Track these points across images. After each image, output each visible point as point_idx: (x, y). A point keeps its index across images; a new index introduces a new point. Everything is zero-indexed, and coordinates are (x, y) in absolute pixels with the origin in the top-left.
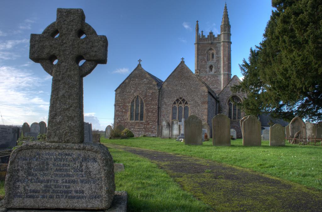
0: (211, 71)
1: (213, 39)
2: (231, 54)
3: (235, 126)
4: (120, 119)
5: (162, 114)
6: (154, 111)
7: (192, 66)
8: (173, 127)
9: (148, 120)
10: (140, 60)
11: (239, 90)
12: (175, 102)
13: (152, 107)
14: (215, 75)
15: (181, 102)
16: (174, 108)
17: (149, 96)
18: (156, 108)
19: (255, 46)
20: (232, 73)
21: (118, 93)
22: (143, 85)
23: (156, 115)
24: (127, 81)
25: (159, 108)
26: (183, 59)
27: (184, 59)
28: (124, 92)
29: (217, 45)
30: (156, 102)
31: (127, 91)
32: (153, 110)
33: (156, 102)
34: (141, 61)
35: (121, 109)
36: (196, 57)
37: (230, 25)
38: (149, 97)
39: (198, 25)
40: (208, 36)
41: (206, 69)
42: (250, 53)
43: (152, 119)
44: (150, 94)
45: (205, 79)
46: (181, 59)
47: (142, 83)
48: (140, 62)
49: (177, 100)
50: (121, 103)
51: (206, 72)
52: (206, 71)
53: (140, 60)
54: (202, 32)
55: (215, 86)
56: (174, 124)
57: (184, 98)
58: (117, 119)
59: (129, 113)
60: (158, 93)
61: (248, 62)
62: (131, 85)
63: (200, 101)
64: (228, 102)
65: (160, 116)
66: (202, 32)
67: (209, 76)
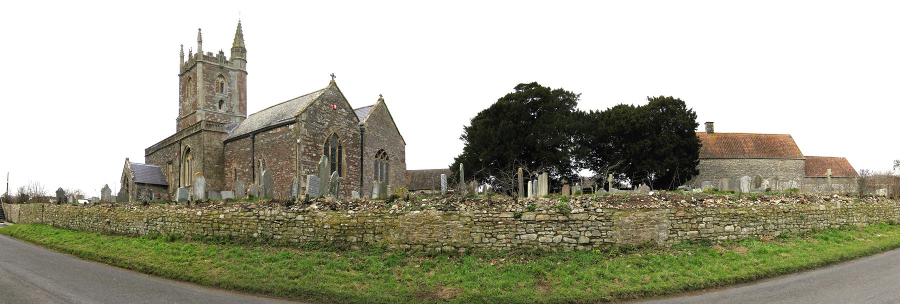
16: (376, 166)
35: (310, 151)
39: (200, 34)
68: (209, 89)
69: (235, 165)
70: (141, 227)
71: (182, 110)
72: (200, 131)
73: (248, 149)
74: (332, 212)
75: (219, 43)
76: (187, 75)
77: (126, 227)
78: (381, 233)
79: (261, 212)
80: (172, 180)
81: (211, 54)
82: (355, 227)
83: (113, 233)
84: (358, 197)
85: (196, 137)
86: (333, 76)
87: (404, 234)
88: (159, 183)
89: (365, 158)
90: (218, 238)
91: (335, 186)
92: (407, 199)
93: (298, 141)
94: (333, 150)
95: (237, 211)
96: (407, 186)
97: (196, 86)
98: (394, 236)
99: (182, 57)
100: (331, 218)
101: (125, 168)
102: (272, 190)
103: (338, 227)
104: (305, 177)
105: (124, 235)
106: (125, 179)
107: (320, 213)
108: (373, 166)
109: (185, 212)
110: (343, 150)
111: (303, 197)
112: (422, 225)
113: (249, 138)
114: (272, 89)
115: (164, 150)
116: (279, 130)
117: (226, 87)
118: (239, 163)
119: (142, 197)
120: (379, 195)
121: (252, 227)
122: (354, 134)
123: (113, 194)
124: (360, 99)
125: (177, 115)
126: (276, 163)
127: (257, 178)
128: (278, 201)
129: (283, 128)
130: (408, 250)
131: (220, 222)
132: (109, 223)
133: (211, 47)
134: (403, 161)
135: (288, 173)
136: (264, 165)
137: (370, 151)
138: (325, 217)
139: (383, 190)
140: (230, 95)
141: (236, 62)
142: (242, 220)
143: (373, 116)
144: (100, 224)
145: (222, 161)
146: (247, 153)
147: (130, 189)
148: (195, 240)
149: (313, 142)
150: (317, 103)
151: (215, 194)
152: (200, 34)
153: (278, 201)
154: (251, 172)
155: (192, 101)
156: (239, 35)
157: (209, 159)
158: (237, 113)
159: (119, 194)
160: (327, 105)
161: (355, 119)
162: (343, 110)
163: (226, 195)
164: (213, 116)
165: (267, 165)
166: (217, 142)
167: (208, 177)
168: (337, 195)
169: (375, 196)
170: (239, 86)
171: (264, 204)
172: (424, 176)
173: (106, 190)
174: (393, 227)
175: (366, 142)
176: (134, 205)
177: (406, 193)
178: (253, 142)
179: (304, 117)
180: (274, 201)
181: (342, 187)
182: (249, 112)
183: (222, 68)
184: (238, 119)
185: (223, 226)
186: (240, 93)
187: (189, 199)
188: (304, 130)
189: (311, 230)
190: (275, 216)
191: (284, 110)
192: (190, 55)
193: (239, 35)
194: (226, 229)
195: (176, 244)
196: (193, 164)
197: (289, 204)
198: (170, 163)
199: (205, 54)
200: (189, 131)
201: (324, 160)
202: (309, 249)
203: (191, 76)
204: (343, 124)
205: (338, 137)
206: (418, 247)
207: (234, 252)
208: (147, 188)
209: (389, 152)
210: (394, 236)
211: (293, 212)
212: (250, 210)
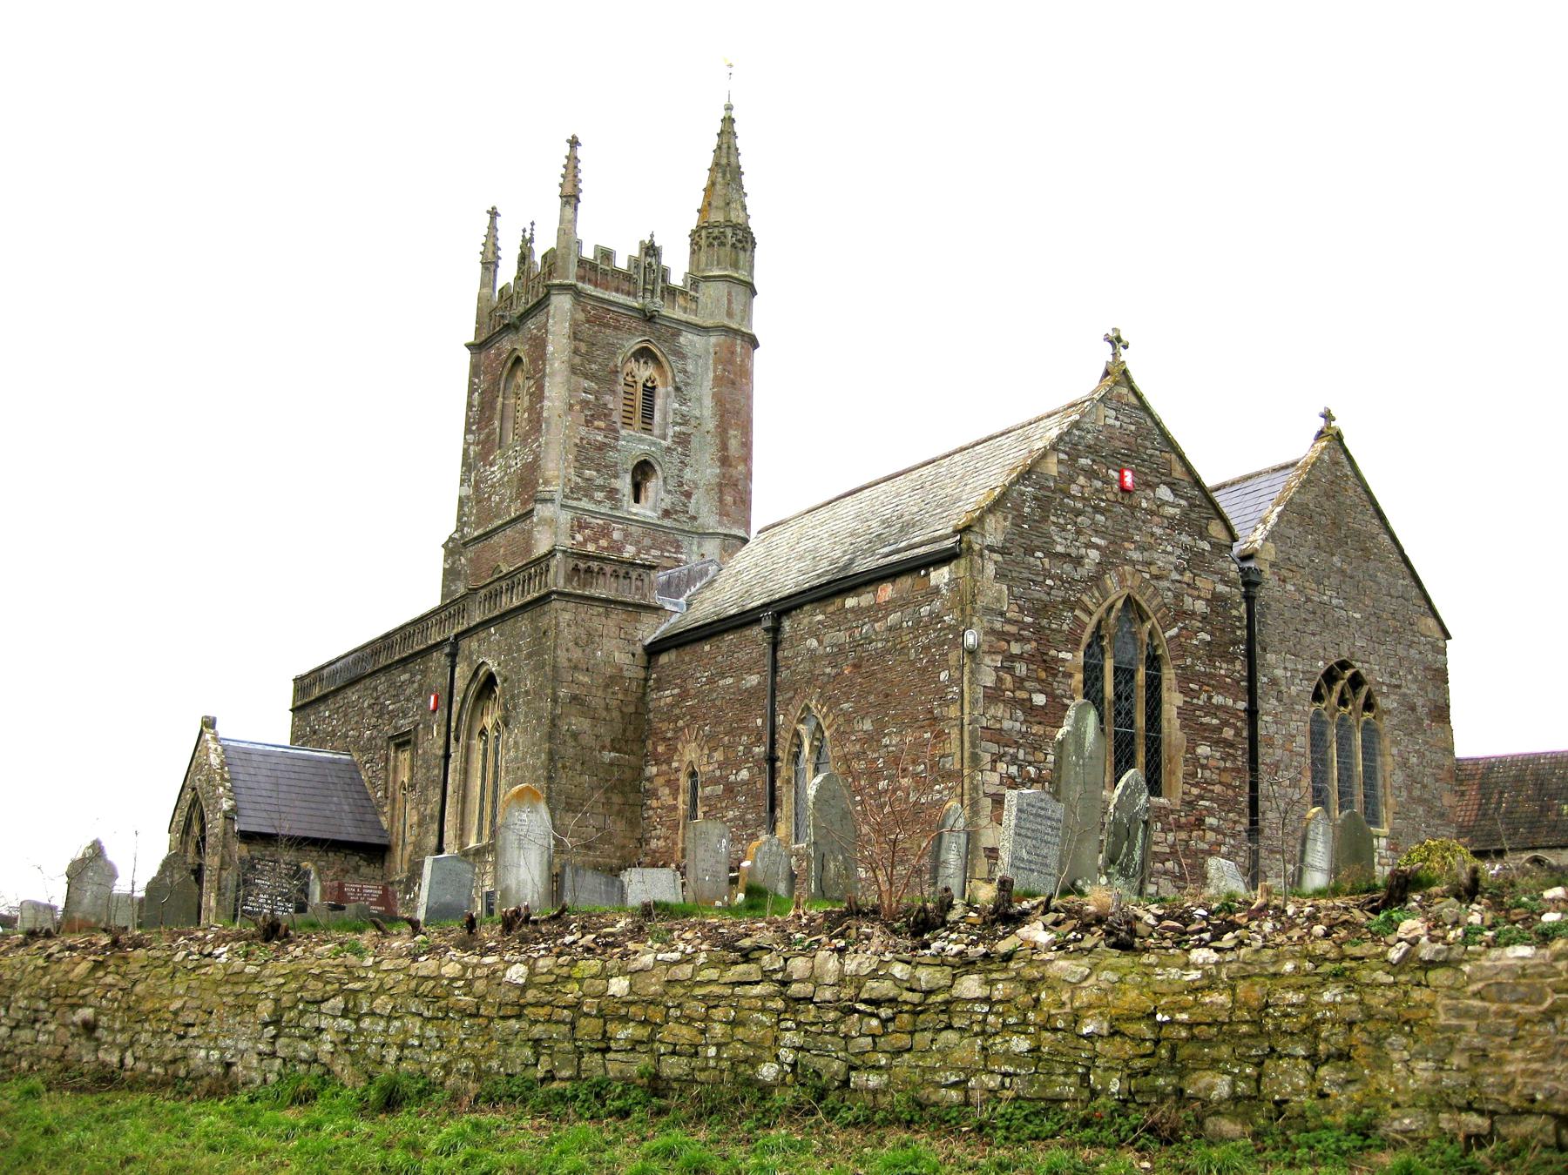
0: (637, 500)
4: (1013, 770)
6: (1228, 733)
9: (1195, 791)
16: (1317, 739)
17: (1194, 613)
21: (991, 549)
23: (1242, 760)
28: (1030, 551)
29: (682, 339)
31: (1060, 549)
32: (1225, 723)
33: (1238, 666)
35: (1020, 683)
39: (572, 164)
40: (634, 262)
41: (616, 477)
47: (1152, 513)
50: (1020, 639)
52: (616, 491)
58: (993, 769)
68: (595, 413)
69: (690, 753)
70: (243, 1046)
71: (473, 503)
72: (543, 600)
73: (753, 680)
74: (1114, 957)
75: (643, 212)
76: (506, 344)
77: (173, 1047)
78: (1343, 1056)
79: (799, 966)
80: (405, 822)
81: (607, 255)
82: (1224, 1028)
83: (107, 1080)
84: (1238, 886)
85: (524, 624)
86: (1116, 341)
87: (1456, 1060)
88: (349, 833)
89: (1268, 705)
90: (599, 1092)
91: (1130, 836)
92: (1470, 891)
93: (970, 639)
94: (1124, 674)
95: (688, 959)
96: (1463, 831)
97: (538, 395)
98: (1409, 1071)
99: (490, 265)
100: (1113, 988)
101: (196, 763)
102: (849, 867)
103: (1143, 1028)
104: (998, 801)
105: (158, 1085)
106: (191, 818)
107: (1063, 966)
108: (1302, 742)
109: (451, 969)
110: (1169, 675)
111: (986, 893)
112: (1548, 1016)
113: (756, 632)
114: (860, 420)
115: (381, 682)
116: (887, 591)
117: (664, 401)
118: (712, 742)
119: (261, 903)
120: (1334, 871)
121: (754, 1032)
122: (1215, 600)
123: (121, 886)
124: (1236, 440)
125: (448, 526)
126: (872, 739)
127: (785, 811)
128: (874, 914)
129: (906, 582)
130: (1477, 1140)
131: (612, 1012)
132: (89, 1027)
133: (612, 230)
134: (1441, 713)
135: (922, 784)
136: (818, 751)
137: (1288, 673)
138: (1084, 980)
139: (1353, 848)
140: (683, 440)
141: (711, 294)
142: (712, 1002)
143: (1296, 513)
144: (44, 1037)
145: (637, 731)
146: (746, 699)
147: (211, 861)
148: (492, 1100)
149: (1034, 640)
150: (1052, 467)
151: (591, 881)
152: (572, 164)
153: (874, 914)
154: (762, 784)
155: (517, 464)
156: (726, 170)
157: (578, 723)
158: (709, 519)
159: (153, 887)
160: (1091, 474)
161: (1216, 529)
162: (1164, 493)
163: (647, 885)
164: (605, 532)
165: (831, 751)
166: (619, 648)
167: (561, 804)
168: (1140, 878)
169: (1316, 879)
170: (719, 401)
171: (811, 928)
172: (1540, 785)
173: (90, 866)
174: (1405, 1023)
175: (1270, 630)
176: (221, 939)
177: (1462, 862)
178: (775, 645)
179: (995, 531)
180: (856, 912)
181: (1163, 840)
182: (760, 515)
183: (649, 317)
184: (711, 547)
185: (623, 1033)
186: (723, 430)
187: (479, 908)
188: (994, 591)
189: (1021, 1044)
190: (858, 980)
191: (911, 506)
192: (524, 258)
193: (726, 170)
194: (635, 1044)
195: (404, 1122)
196: (507, 747)
197: (924, 925)
198: (403, 741)
199: (588, 253)
200: (494, 596)
201: (1079, 720)
202: (1012, 1134)
203: (523, 350)
204: (1166, 558)
205: (1143, 617)
206: (1529, 1125)
207: (669, 1153)
208: (287, 856)
209: (1373, 671)
210: (1409, 1071)
211: (940, 961)
212: (747, 956)
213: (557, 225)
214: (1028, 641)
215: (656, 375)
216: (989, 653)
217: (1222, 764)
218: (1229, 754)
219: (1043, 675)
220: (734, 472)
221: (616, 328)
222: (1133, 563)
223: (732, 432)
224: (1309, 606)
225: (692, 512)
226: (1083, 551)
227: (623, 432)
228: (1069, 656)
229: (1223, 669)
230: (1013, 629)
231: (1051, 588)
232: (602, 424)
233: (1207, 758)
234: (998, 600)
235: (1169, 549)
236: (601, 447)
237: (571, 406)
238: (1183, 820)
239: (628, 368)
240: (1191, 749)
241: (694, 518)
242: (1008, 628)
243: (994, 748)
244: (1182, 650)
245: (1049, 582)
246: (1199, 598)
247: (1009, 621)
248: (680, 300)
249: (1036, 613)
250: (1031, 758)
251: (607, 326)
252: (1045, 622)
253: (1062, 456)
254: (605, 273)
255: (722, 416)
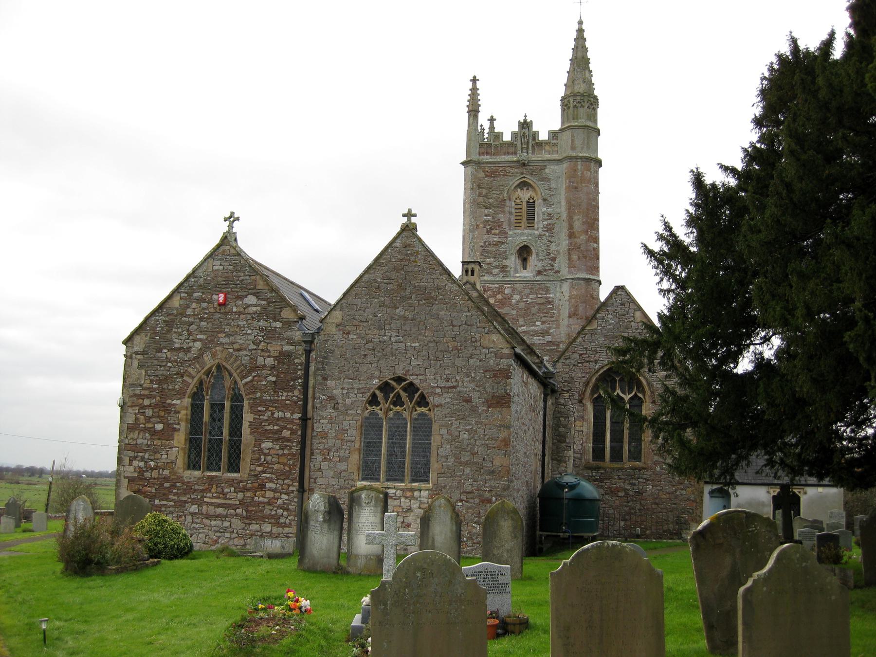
0: (525, 268)
1: (533, 146)
2: (598, 203)
3: (618, 489)
5: (318, 445)
6: (286, 433)
7: (448, 247)
8: (355, 519)
9: (259, 469)
10: (232, 213)
11: (651, 362)
12: (374, 396)
13: (278, 414)
14: (539, 283)
15: (398, 396)
16: (371, 427)
17: (264, 366)
18: (292, 421)
19: (721, 166)
20: (602, 278)
21: (137, 353)
22: (241, 323)
23: (296, 449)
24: (398, 244)
25: (305, 419)
26: (409, 215)
27: (415, 215)
28: (160, 350)
30: (296, 392)
31: (177, 346)
33: (296, 392)
34: (238, 219)
35: (148, 419)
36: (468, 213)
37: (596, 98)
38: (265, 372)
39: (474, 92)
40: (514, 135)
41: (506, 259)
42: (689, 193)
43: (276, 467)
44: (270, 361)
45: (499, 297)
46: (404, 215)
47: (239, 313)
48: (231, 226)
49: (385, 388)
50: (149, 397)
51: (504, 269)
52: (506, 266)
53: (232, 213)
54: (492, 120)
55: (538, 323)
56: (360, 505)
57: (411, 378)
58: (131, 464)
59: (180, 438)
60: (303, 359)
61: (686, 235)
62: (191, 319)
63: (477, 394)
64: (593, 392)
65: (312, 454)
66: (492, 120)
67: (519, 286)
75: (531, 102)
117: (540, 209)
140: (550, 228)
152: (474, 92)
160: (200, 300)
162: (251, 300)
164: (500, 290)
213: (466, 128)
214: (155, 397)
215: (534, 195)
216: (132, 406)
217: (281, 452)
218: (287, 446)
219: (162, 414)
220: (578, 240)
221: (504, 175)
222: (222, 344)
223: (575, 218)
224: (370, 345)
225: (556, 268)
226: (191, 344)
227: (511, 233)
228: (178, 402)
229: (283, 396)
230: (146, 392)
231: (170, 367)
232: (497, 231)
233: (269, 449)
234: (139, 379)
235: (249, 331)
236: (497, 244)
237: (478, 226)
238: (249, 486)
239: (516, 195)
240: (258, 443)
241: (558, 272)
242: (143, 392)
243: (131, 454)
244: (252, 388)
245: (169, 364)
246: (269, 356)
247: (145, 389)
248: (547, 148)
249: (160, 382)
250: (152, 457)
251: (500, 175)
252: (165, 386)
253: (183, 295)
254: (496, 147)
255: (569, 209)
